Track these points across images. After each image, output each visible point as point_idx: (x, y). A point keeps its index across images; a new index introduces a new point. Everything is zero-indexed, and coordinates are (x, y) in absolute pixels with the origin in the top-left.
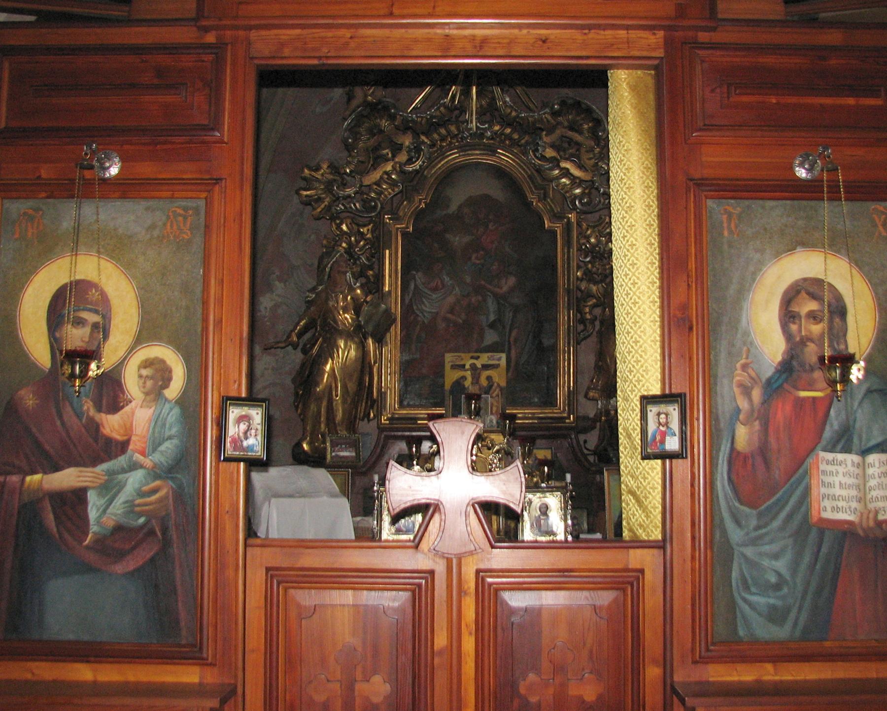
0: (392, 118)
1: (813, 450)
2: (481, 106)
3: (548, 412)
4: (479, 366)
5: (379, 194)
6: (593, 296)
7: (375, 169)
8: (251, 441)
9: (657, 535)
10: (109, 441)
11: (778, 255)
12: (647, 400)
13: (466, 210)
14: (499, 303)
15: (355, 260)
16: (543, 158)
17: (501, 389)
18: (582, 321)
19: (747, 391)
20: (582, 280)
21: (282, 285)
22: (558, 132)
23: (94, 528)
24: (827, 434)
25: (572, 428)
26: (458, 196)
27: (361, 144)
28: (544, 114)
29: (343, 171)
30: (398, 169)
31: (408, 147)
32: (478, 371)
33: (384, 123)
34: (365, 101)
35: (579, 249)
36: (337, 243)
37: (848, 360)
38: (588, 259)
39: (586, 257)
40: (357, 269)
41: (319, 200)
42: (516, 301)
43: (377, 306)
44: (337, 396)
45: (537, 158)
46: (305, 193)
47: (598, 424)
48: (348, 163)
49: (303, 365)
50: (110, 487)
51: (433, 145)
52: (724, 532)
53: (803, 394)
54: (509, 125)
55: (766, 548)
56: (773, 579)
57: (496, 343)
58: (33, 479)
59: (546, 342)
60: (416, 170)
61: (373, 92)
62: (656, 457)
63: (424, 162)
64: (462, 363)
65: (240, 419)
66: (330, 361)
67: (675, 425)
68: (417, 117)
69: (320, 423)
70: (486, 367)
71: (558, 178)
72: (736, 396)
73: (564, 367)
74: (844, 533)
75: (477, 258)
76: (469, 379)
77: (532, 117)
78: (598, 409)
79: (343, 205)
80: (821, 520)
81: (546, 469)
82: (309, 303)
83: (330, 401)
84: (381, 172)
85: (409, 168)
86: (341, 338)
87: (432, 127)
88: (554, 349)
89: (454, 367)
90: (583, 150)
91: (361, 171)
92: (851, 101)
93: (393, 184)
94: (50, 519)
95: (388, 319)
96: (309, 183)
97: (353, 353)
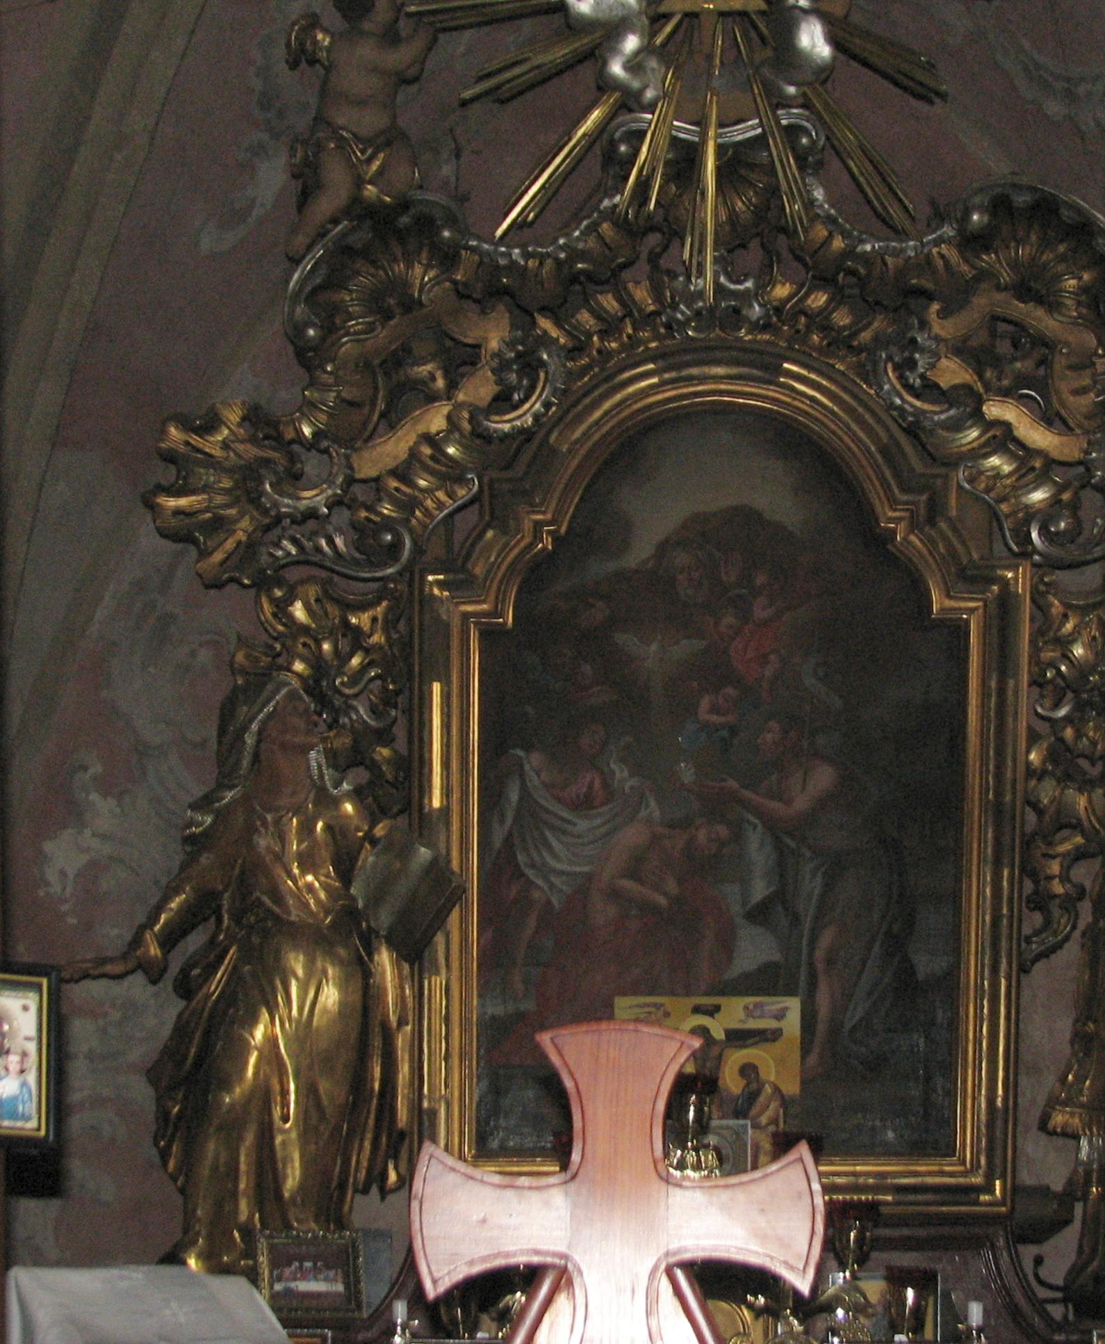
0: (447, 258)
2: (733, 217)
4: (719, 1034)
5: (408, 505)
6: (1077, 826)
7: (392, 427)
13: (682, 558)
14: (780, 848)
15: (336, 713)
16: (929, 390)
17: (785, 1102)
18: (1039, 902)
20: (1041, 775)
21: (112, 802)
22: (983, 302)
25: (994, 1219)
26: (657, 515)
27: (347, 347)
28: (937, 242)
29: (289, 434)
30: (466, 426)
31: (498, 355)
33: (421, 275)
34: (356, 200)
35: (1038, 682)
36: (279, 664)
38: (1062, 712)
39: (1056, 706)
40: (342, 742)
41: (218, 525)
43: (405, 853)
44: (285, 1119)
45: (909, 388)
46: (172, 503)
47: (1078, 1208)
48: (307, 408)
49: (181, 1030)
51: (577, 350)
54: (824, 280)
59: (926, 964)
60: (522, 431)
61: (381, 172)
63: (547, 405)
66: (265, 1016)
68: (527, 256)
69: (234, 1195)
70: (738, 1037)
73: (978, 1041)
75: (714, 709)
77: (896, 253)
78: (1077, 1161)
79: (294, 541)
81: (910, 1293)
82: (195, 844)
83: (266, 1133)
84: (412, 439)
85: (502, 425)
86: (296, 947)
87: (574, 286)
90: (1060, 363)
91: (348, 433)
93: (451, 474)
95: (441, 887)
96: (182, 469)
97: (331, 996)
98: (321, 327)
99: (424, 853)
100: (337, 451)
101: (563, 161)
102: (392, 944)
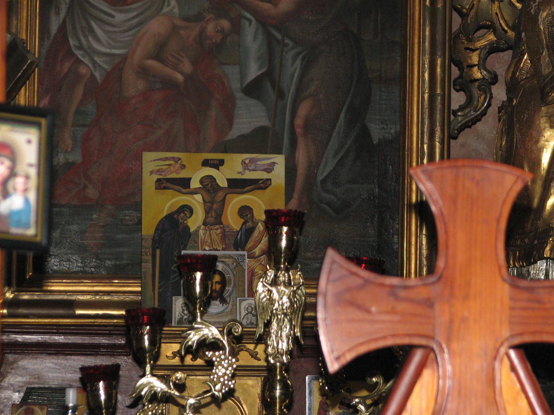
4: (223, 183)
14: (269, 37)
32: (220, 195)
57: (260, 131)
59: (377, 132)
64: (183, 174)
70: (238, 185)
76: (199, 214)
89: (163, 184)
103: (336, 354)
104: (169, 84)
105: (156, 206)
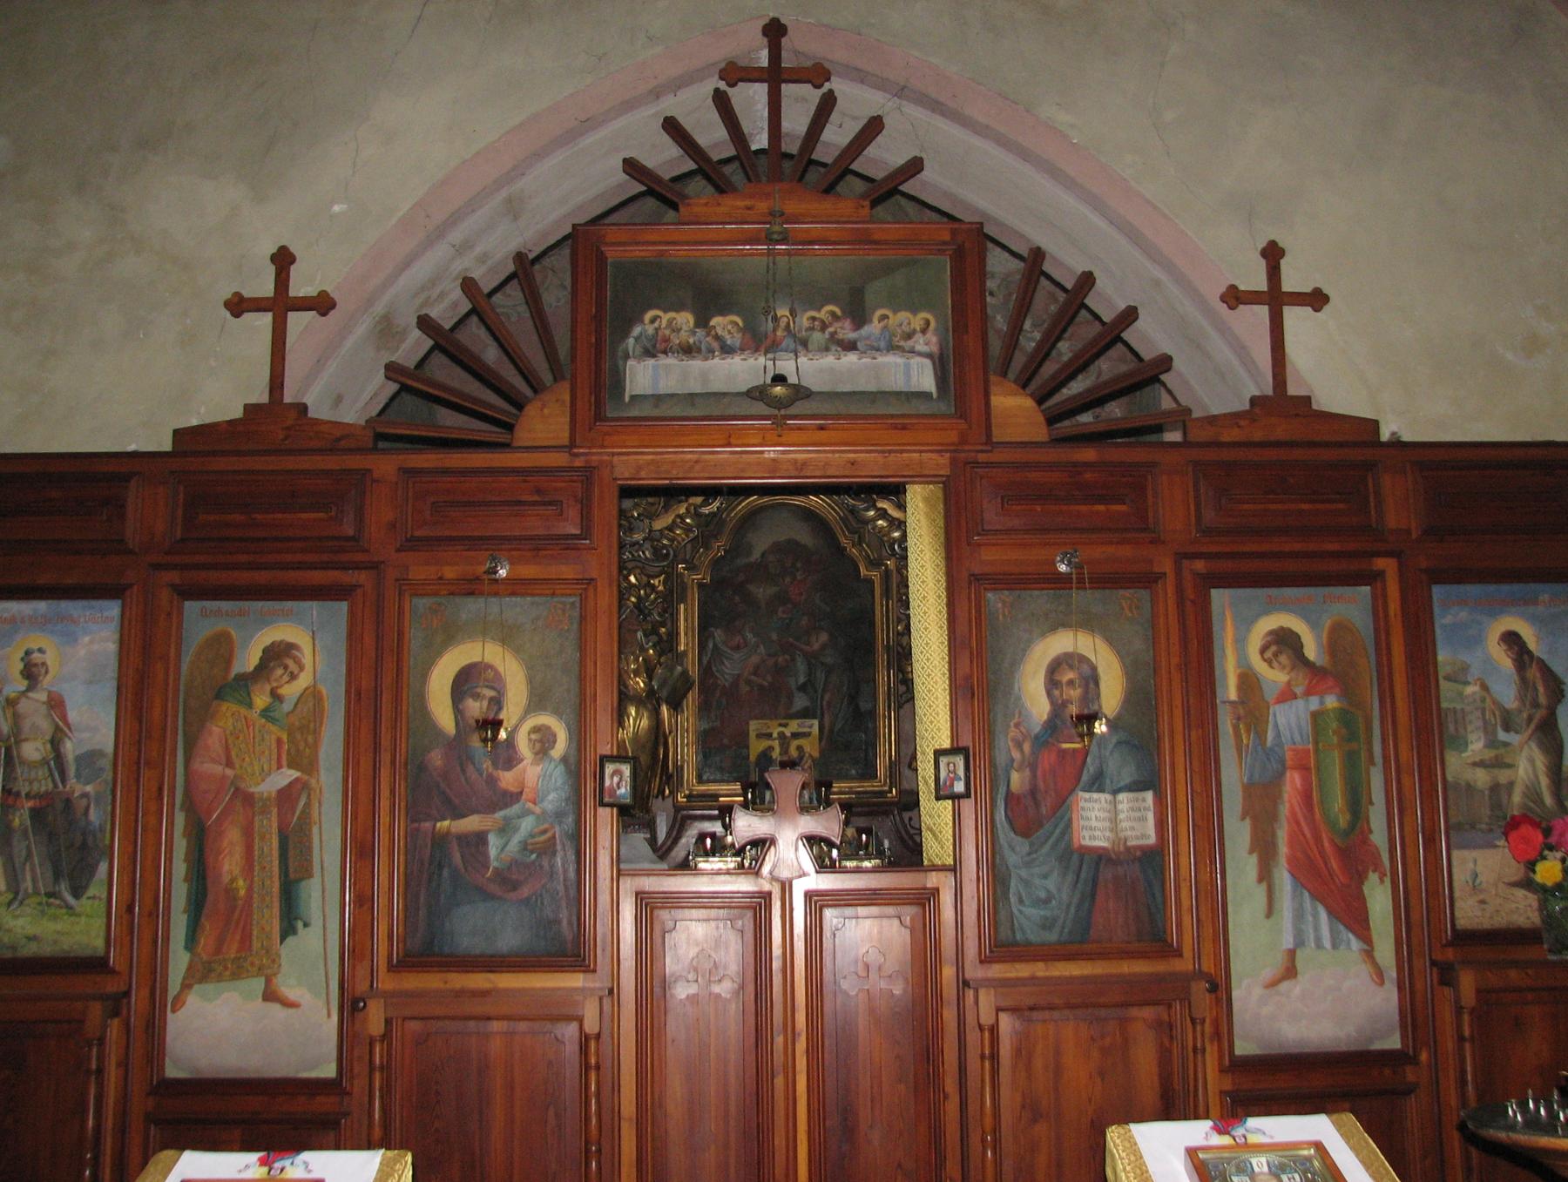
1: (1073, 791)
3: (868, 786)
5: (672, 540)
8: (623, 790)
9: (950, 861)
10: (505, 793)
11: (1043, 635)
12: (938, 753)
13: (771, 558)
14: (809, 664)
19: (1019, 745)
23: (494, 864)
24: (1085, 778)
25: (892, 804)
26: (761, 542)
37: (1091, 718)
42: (829, 660)
43: (672, 669)
50: (505, 829)
52: (1003, 858)
53: (1065, 746)
55: (1036, 870)
56: (1043, 895)
57: (806, 709)
58: (444, 824)
59: (864, 706)
62: (947, 798)
65: (615, 772)
67: (961, 772)
70: (795, 735)
71: (875, 519)
72: (1008, 749)
74: (1100, 858)
76: (777, 750)
80: (1082, 847)
85: (705, 510)
88: (873, 714)
89: (759, 736)
92: (1101, 508)
93: (688, 529)
94: (457, 857)
97: (645, 723)
98: (494, 559)
99: (679, 668)
100: (647, 521)
101: (301, 566)
102: (668, 703)
103: (35, 874)
104: (761, 686)
105: (756, 747)
